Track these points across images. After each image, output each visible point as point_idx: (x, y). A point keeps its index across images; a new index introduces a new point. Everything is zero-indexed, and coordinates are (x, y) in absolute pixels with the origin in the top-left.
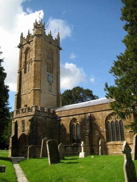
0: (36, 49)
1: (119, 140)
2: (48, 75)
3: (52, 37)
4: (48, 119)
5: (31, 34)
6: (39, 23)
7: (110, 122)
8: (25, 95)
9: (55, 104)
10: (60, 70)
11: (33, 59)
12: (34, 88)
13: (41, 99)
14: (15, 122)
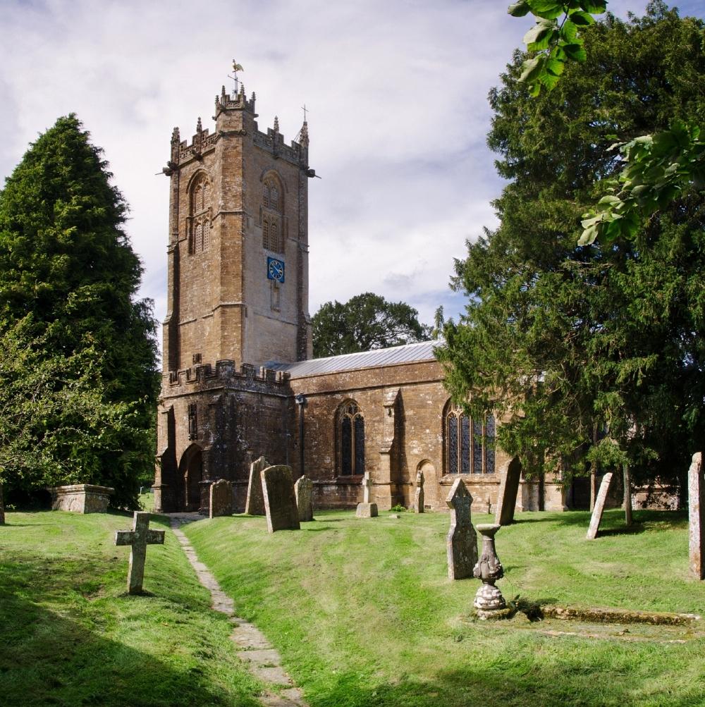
0: (225, 176)
1: (480, 470)
2: (269, 258)
3: (281, 137)
4: (266, 400)
6: (233, 98)
7: (458, 417)
8: (193, 324)
9: (292, 350)
10: (307, 242)
11: (216, 211)
12: (222, 299)
13: (246, 335)
14: (168, 410)
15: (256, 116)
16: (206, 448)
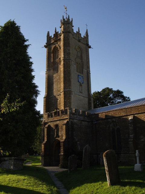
4: (83, 122)
5: (58, 32)
6: (66, 20)
15: (73, 26)
16: (62, 141)
